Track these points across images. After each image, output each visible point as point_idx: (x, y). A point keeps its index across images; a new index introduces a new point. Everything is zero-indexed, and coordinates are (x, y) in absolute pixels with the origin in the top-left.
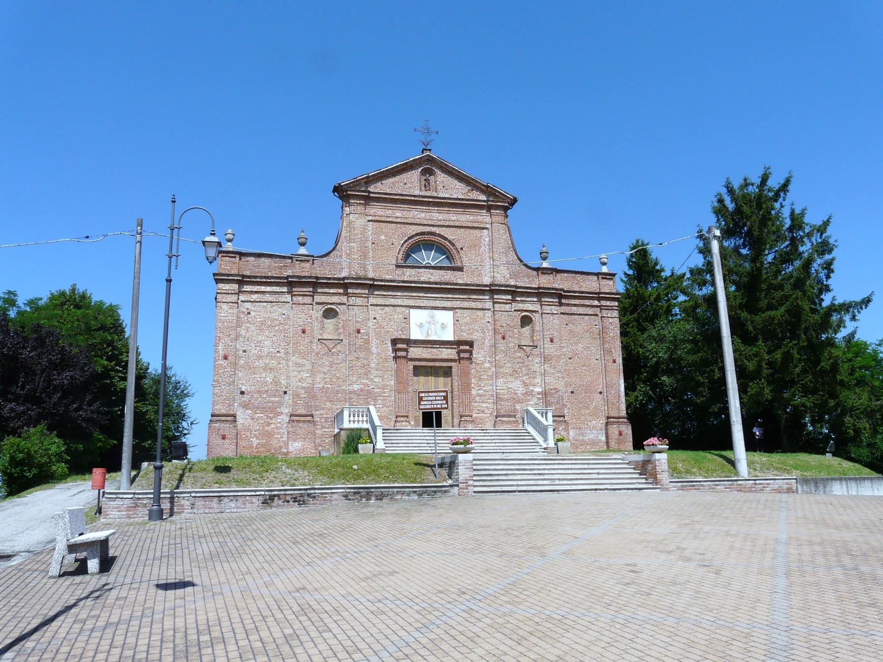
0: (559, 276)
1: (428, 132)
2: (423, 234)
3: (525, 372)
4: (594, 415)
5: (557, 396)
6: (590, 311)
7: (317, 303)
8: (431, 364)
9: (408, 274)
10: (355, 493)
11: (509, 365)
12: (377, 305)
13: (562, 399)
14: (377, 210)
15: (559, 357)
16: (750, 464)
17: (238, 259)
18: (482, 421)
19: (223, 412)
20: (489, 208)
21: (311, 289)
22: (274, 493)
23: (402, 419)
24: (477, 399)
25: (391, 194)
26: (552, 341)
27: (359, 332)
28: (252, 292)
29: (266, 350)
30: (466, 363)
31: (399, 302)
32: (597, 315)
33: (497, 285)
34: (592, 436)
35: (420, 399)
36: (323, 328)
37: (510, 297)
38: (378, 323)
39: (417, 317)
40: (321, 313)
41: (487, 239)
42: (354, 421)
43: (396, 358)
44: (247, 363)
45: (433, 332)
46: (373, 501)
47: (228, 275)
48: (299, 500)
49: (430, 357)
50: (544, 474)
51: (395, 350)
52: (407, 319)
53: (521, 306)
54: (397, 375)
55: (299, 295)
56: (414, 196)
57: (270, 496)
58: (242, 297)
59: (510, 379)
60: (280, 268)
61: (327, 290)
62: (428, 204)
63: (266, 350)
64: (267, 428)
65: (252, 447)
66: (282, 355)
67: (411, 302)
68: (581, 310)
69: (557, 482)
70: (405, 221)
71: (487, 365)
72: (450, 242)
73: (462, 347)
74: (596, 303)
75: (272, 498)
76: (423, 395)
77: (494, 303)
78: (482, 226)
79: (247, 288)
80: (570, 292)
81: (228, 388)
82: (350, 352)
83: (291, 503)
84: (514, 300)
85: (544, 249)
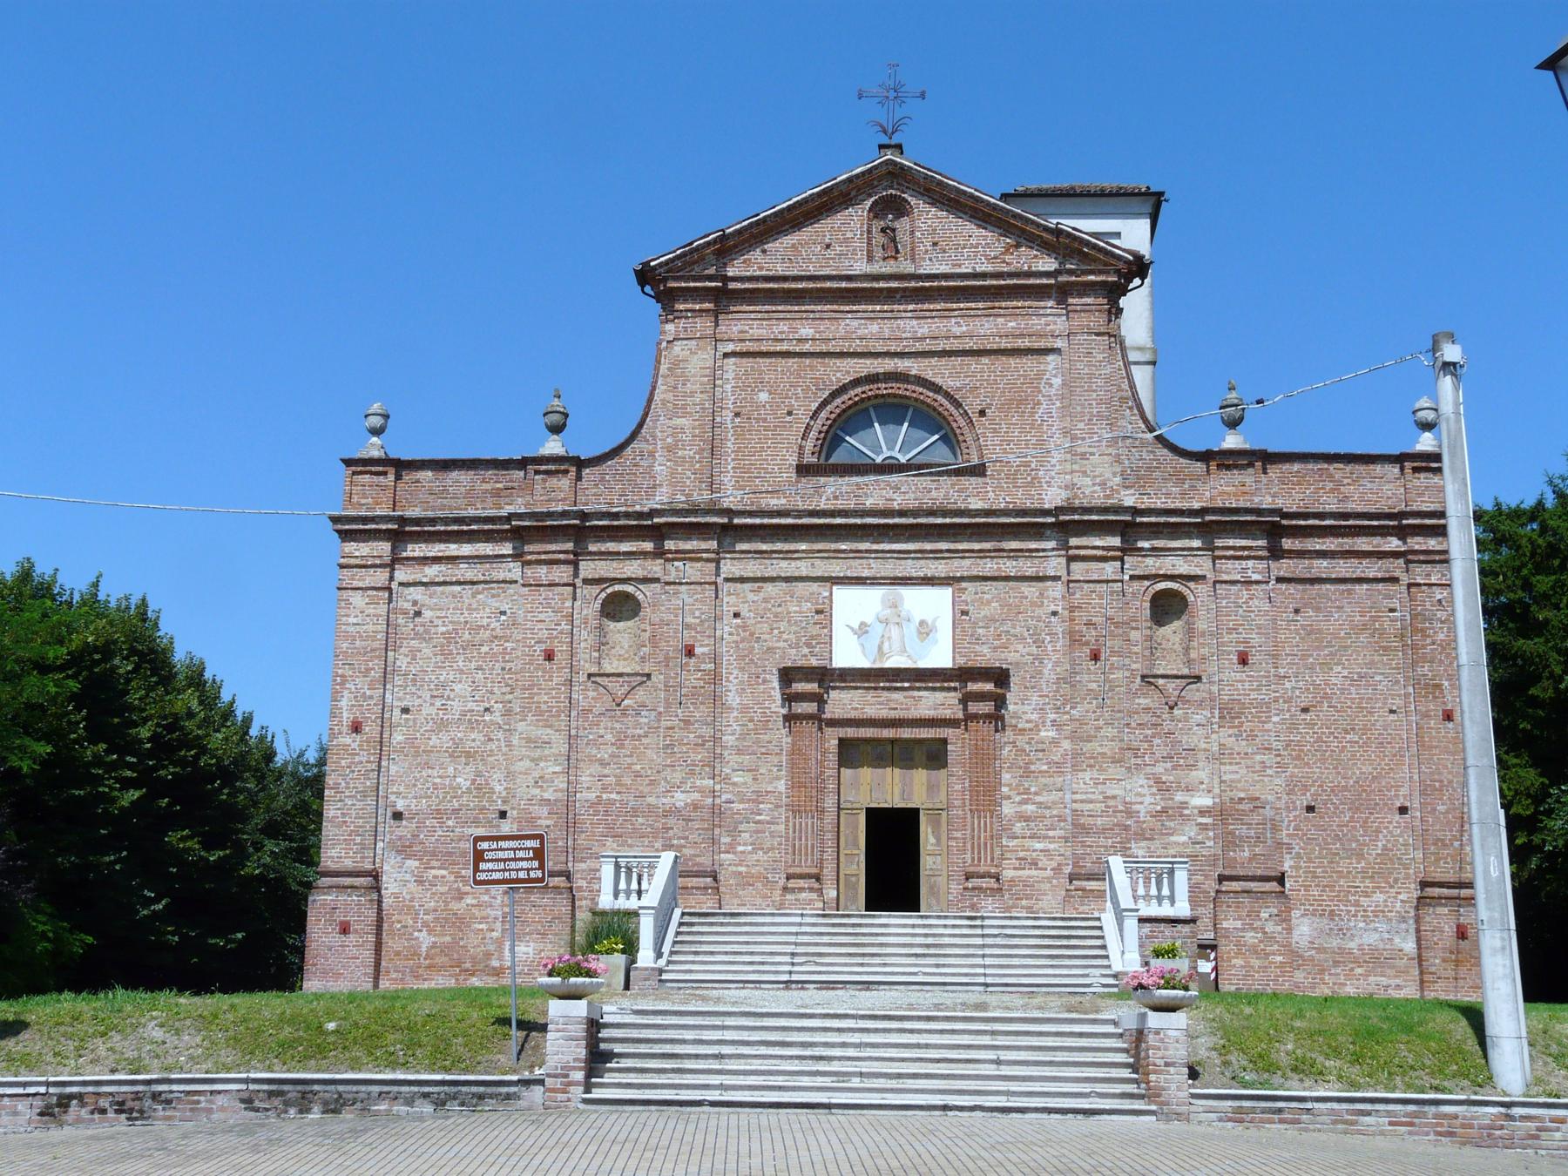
0: (1275, 471)
1: (896, 94)
2: (872, 379)
3: (1161, 751)
4: (1382, 874)
5: (1256, 818)
6: (1372, 569)
7: (586, 581)
8: (888, 733)
9: (830, 490)
10: (271, 1094)
11: (1110, 732)
12: (742, 580)
13: (1275, 829)
14: (747, 325)
15: (1265, 707)
16: (1538, 1042)
17: (391, 477)
18: (1028, 890)
19: (348, 864)
20: (1062, 293)
21: (570, 546)
22: (69, 1090)
23: (802, 883)
24: (1018, 827)
25: (785, 279)
26: (1243, 660)
27: (690, 652)
28: (425, 561)
29: (456, 706)
30: (986, 728)
31: (803, 568)
32: (1395, 580)
33: (1073, 510)
34: (1371, 939)
35: (479, 856)
36: (601, 644)
37: (1116, 541)
38: (744, 627)
39: (853, 607)
40: (598, 606)
41: (1057, 381)
42: (628, 893)
43: (789, 718)
44: (411, 741)
45: (896, 646)
46: (315, 1115)
47: (365, 520)
48: (131, 1108)
49: (884, 713)
50: (830, 1059)
51: (789, 699)
52: (823, 613)
53: (1151, 564)
54: (793, 765)
55: (539, 562)
56: (849, 278)
57: (60, 1096)
58: (401, 574)
59: (1115, 771)
60: (497, 493)
61: (611, 546)
62: (889, 296)
63: (456, 706)
64: (454, 906)
65: (416, 954)
66: (497, 717)
67: (836, 568)
68: (1343, 568)
69: (855, 1082)
70: (824, 348)
71: (1048, 733)
72: (947, 395)
73: (973, 687)
74: (1394, 544)
75: (64, 1102)
76: (485, 845)
77: (1071, 559)
78: (1042, 344)
79: (415, 550)
80: (1306, 516)
81: (360, 805)
82: (668, 705)
83: (111, 1115)
84: (1128, 549)
85: (1233, 396)
